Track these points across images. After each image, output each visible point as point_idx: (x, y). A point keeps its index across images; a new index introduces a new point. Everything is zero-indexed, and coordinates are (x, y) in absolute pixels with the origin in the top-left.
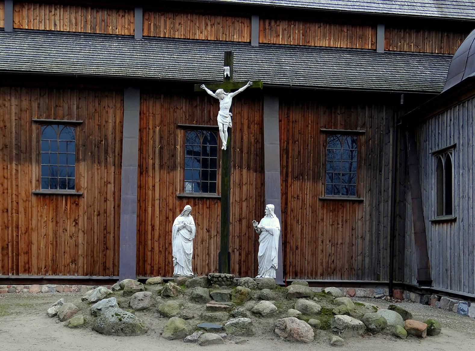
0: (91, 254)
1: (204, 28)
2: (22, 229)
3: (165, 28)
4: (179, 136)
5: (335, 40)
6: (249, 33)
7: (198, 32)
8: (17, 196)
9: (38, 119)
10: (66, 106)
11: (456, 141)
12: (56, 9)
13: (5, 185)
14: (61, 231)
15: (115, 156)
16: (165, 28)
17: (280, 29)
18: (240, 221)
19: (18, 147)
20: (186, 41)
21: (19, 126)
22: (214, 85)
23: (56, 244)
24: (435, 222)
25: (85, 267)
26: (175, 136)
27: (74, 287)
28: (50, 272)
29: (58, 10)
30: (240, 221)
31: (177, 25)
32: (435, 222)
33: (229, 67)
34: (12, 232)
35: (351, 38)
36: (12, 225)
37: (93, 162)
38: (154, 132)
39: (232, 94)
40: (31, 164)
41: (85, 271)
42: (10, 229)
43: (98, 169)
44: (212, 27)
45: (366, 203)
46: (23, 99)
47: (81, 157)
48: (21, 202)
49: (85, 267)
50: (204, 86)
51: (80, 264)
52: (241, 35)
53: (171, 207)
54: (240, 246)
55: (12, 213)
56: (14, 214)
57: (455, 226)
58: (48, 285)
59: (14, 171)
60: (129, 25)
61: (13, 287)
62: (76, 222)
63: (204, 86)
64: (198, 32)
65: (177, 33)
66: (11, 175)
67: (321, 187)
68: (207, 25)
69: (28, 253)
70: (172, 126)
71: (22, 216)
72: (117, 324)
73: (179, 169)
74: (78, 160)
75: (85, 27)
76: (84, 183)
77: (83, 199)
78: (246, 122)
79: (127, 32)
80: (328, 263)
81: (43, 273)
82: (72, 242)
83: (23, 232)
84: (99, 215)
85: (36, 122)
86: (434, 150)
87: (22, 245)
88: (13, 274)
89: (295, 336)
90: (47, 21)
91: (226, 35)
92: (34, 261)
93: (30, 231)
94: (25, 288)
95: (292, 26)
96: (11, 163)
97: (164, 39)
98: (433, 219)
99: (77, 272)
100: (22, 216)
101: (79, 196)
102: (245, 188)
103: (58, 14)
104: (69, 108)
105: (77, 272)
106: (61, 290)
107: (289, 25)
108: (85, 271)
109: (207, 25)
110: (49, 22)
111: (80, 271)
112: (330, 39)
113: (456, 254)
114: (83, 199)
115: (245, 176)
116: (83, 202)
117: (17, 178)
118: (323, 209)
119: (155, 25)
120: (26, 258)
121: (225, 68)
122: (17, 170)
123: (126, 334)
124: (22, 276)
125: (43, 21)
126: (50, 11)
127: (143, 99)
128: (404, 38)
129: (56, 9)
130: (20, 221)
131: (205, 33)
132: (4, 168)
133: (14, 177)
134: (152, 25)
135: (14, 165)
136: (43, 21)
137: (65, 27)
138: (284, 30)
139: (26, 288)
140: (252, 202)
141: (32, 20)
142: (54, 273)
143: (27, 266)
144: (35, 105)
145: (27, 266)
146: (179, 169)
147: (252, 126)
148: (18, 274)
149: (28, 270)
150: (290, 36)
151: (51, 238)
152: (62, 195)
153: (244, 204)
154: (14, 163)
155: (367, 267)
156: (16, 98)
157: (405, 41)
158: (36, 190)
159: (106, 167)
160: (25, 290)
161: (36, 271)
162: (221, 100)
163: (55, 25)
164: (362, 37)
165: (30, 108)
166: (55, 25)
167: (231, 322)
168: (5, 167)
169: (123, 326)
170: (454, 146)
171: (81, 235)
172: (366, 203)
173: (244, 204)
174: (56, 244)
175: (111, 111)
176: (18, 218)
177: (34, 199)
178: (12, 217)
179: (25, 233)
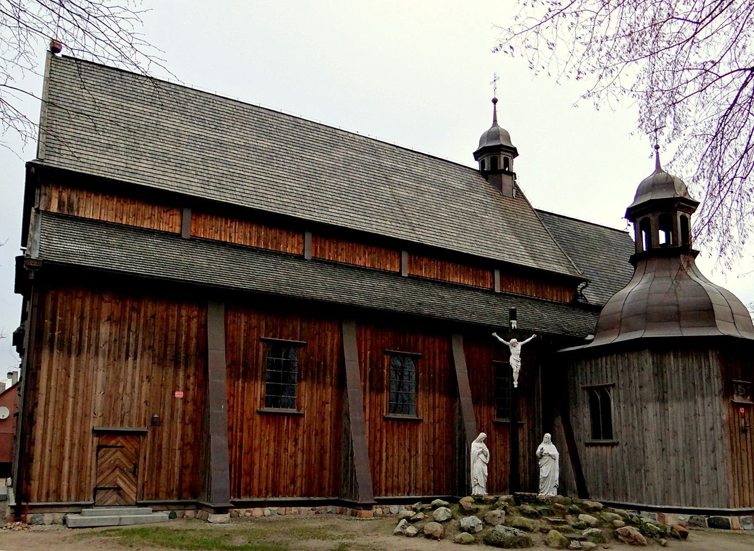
0: (308, 475)
1: (362, 255)
2: (245, 447)
3: (330, 251)
4: (386, 361)
5: (464, 279)
6: (220, 223)
7: (358, 259)
8: (242, 414)
9: (265, 337)
10: (291, 327)
11: (615, 381)
12: (231, 222)
13: (231, 403)
14: (282, 451)
15: (332, 378)
16: (330, 252)
17: (423, 263)
18: (434, 441)
19: (245, 365)
20: (335, 264)
21: (248, 342)
22: (508, 333)
23: (277, 465)
24: (587, 445)
25: (303, 488)
26: (383, 360)
27: (294, 509)
28: (270, 494)
29: (234, 223)
30: (434, 441)
31: (340, 250)
32: (587, 445)
33: (515, 321)
34: (236, 452)
35: (475, 277)
36: (236, 445)
37: (313, 383)
38: (366, 356)
39: (521, 343)
40: (257, 382)
41: (303, 492)
42: (234, 448)
43: (317, 390)
44: (369, 256)
45: (525, 426)
46: (252, 316)
47: (302, 377)
48: (245, 421)
49: (303, 488)
50: (495, 334)
51: (298, 484)
52: (392, 265)
53: (378, 427)
54: (434, 465)
55: (236, 432)
56: (238, 434)
57: (616, 449)
58: (270, 508)
59: (240, 388)
60: (298, 245)
61: (235, 511)
62: (296, 440)
63: (495, 334)
64: (358, 259)
65: (340, 257)
66: (238, 392)
67: (494, 412)
68: (365, 253)
69: (250, 473)
70: (380, 351)
71: (245, 435)
72: (514, 537)
73: (385, 391)
74: (300, 380)
75: (258, 242)
76: (305, 402)
77: (303, 419)
78: (438, 351)
79: (295, 251)
80: (500, 480)
81: (264, 495)
82: (291, 462)
83: (246, 451)
84: (316, 435)
85: (263, 340)
86: (586, 385)
87: (245, 466)
88: (234, 498)
89: (639, 540)
90: (223, 232)
91: (380, 264)
92: (256, 483)
93: (253, 451)
94: (247, 511)
95: (432, 262)
96: (238, 380)
97: (328, 263)
98: (587, 441)
99: (293, 494)
100: (245, 435)
101: (417, 422)
102: (437, 410)
103: (234, 226)
104: (293, 329)
105: (296, 494)
106: (283, 513)
107: (430, 261)
108: (303, 492)
109: (365, 253)
110: (225, 234)
111: (298, 492)
112: (460, 277)
113: (619, 471)
114: (303, 419)
115: (437, 400)
116: (303, 422)
117: (243, 396)
118: (496, 431)
119: (321, 247)
120: (248, 480)
121: (513, 321)
122: (243, 388)
123: (522, 547)
124: (244, 499)
125: (219, 232)
126: (226, 223)
127: (359, 326)
128: (513, 282)
129: (231, 222)
130: (244, 440)
131: (363, 260)
132: (230, 385)
133: (240, 394)
134: (318, 248)
135: (240, 382)
136: (219, 232)
137: (239, 240)
138: (426, 265)
139: (249, 511)
140: (443, 423)
141: (208, 230)
142: (274, 495)
143: (248, 488)
144: (263, 324)
145: (248, 488)
146: (385, 391)
147: (442, 355)
148: (239, 497)
149: (249, 493)
150: (430, 271)
151: (271, 460)
152: (284, 414)
153: (437, 425)
154: (241, 380)
155: (528, 483)
156: (245, 316)
157: (513, 284)
158: (260, 408)
159: (324, 387)
160: (248, 514)
161: (257, 493)
162: (513, 348)
163: (230, 237)
164: (484, 278)
165: (258, 326)
166: (230, 237)
167: (587, 532)
168: (232, 384)
169: (519, 539)
170: (613, 385)
171: (300, 454)
172: (525, 426)
173: (437, 425)
174: (277, 465)
175: (329, 334)
176: (242, 437)
177: (258, 417)
178: (236, 436)
179: (248, 453)
